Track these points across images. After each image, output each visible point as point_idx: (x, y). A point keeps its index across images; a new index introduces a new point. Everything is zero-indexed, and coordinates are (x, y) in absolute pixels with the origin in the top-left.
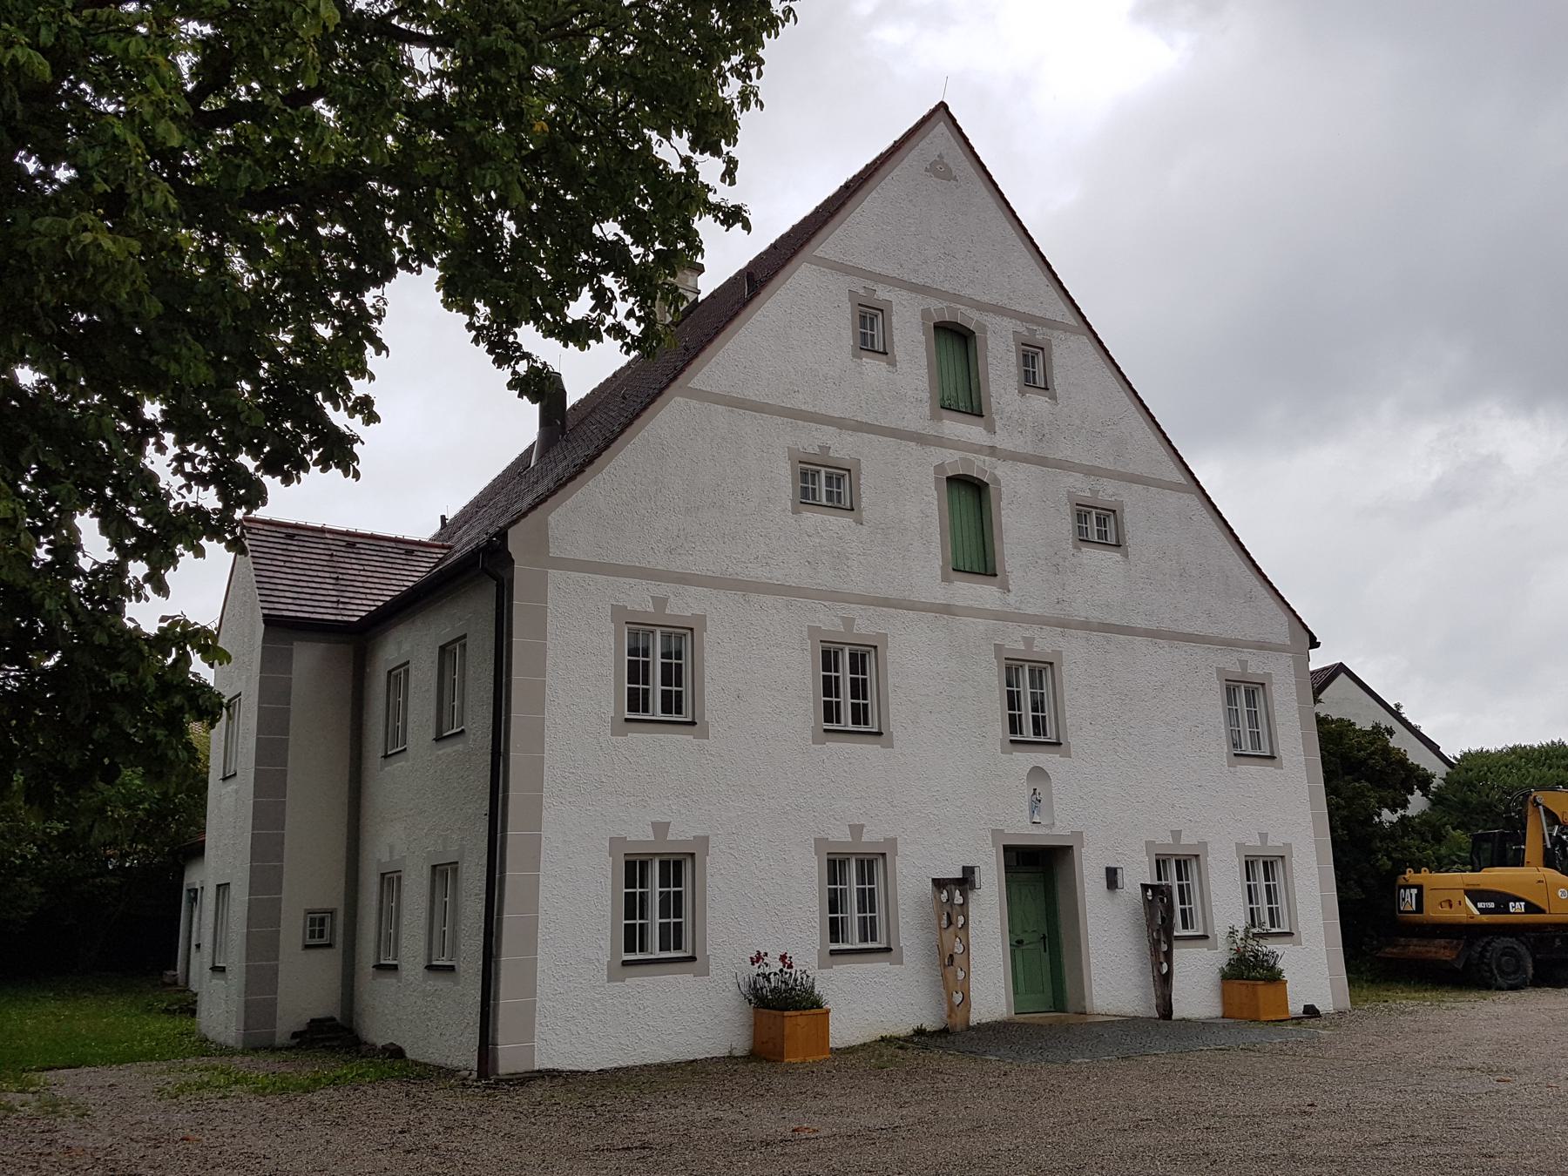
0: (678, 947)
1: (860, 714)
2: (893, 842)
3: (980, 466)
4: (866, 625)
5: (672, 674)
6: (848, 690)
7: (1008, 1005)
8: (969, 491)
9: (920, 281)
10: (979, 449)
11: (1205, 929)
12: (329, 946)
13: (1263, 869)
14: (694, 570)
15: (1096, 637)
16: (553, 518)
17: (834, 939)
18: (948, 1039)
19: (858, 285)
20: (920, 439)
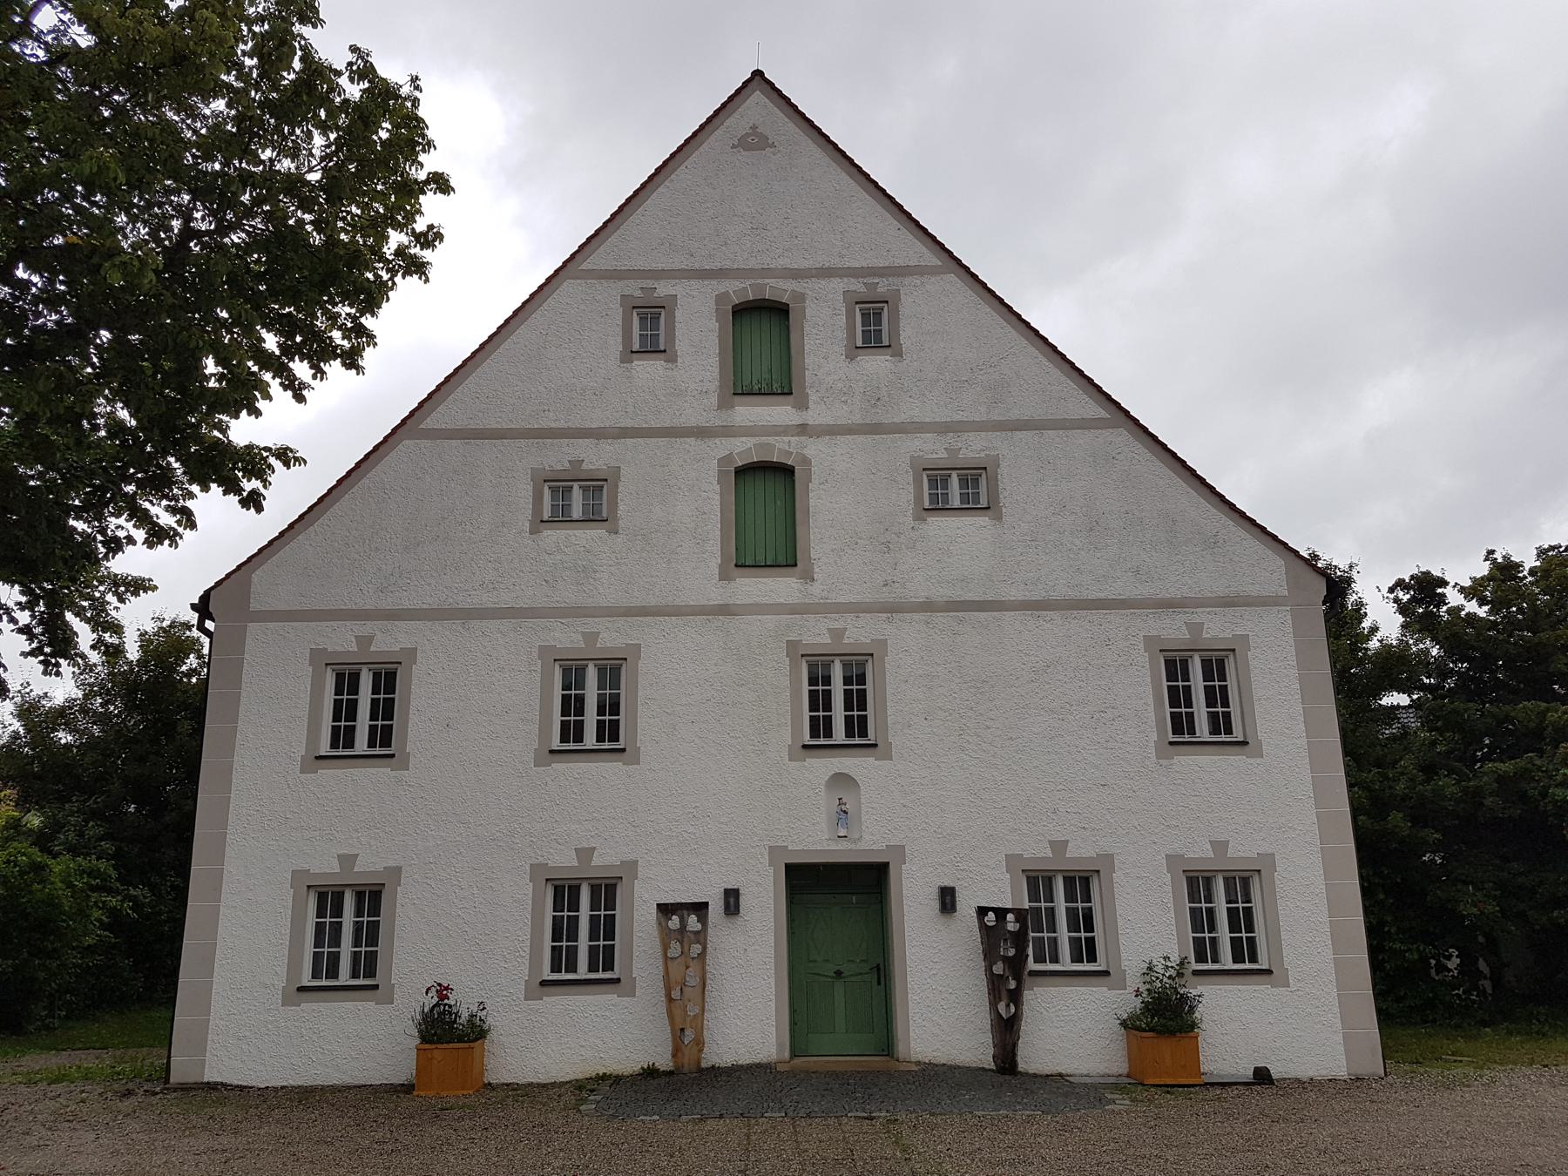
2: (632, 865)
3: (781, 449)
6: (591, 711)
9: (717, 265)
10: (784, 431)
14: (407, 605)
15: (940, 619)
16: (255, 577)
18: (682, 1083)
19: (633, 288)
20: (701, 433)
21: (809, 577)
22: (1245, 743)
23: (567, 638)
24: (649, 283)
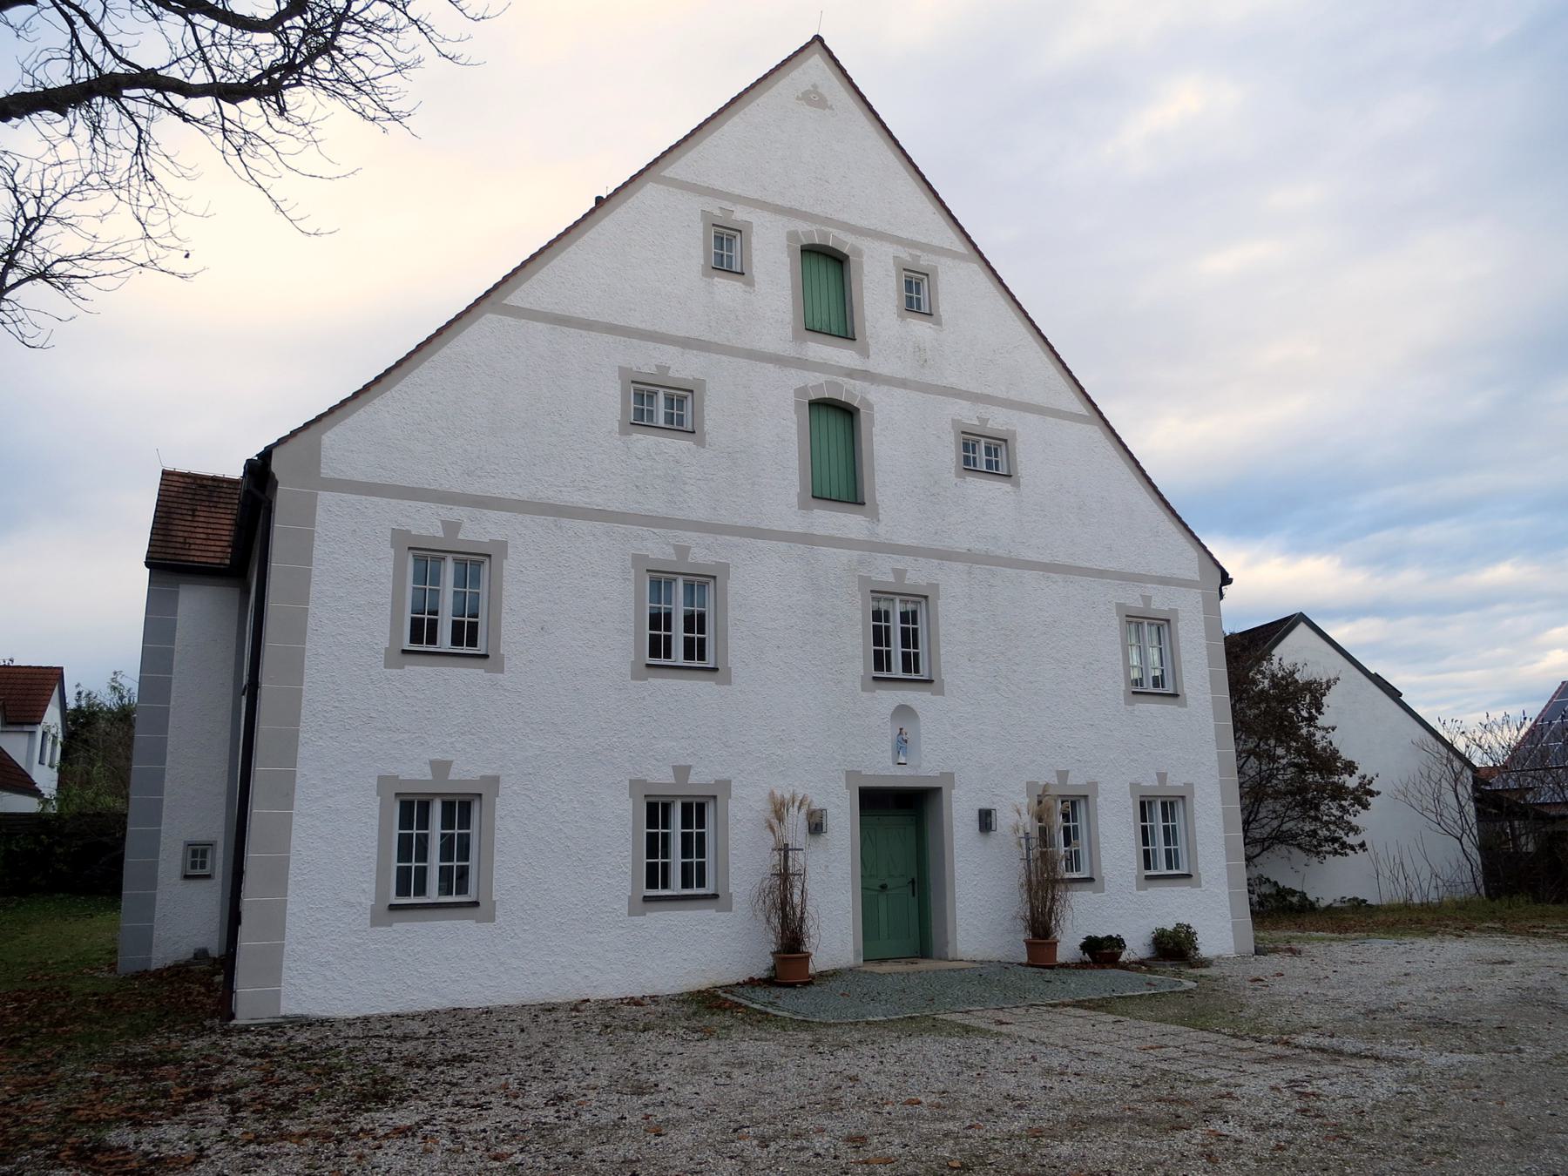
0: (701, 884)
1: (910, 663)
2: (726, 785)
3: (850, 391)
4: (702, 553)
5: (910, 638)
7: (856, 951)
8: (836, 418)
10: (851, 373)
11: (1092, 872)
12: (208, 877)
13: (1160, 814)
14: (497, 493)
17: (1147, 867)
19: (714, 207)
21: (874, 516)
22: (715, 670)
23: (659, 548)
24: (727, 205)
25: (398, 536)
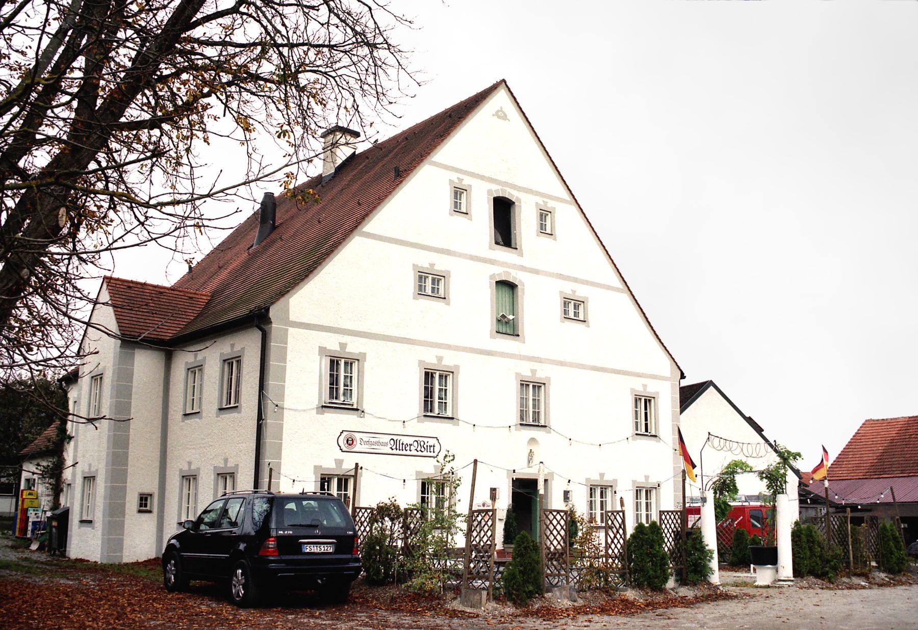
6: (434, 390)
10: (514, 267)
12: (150, 512)
19: (454, 176)
25: (322, 351)
